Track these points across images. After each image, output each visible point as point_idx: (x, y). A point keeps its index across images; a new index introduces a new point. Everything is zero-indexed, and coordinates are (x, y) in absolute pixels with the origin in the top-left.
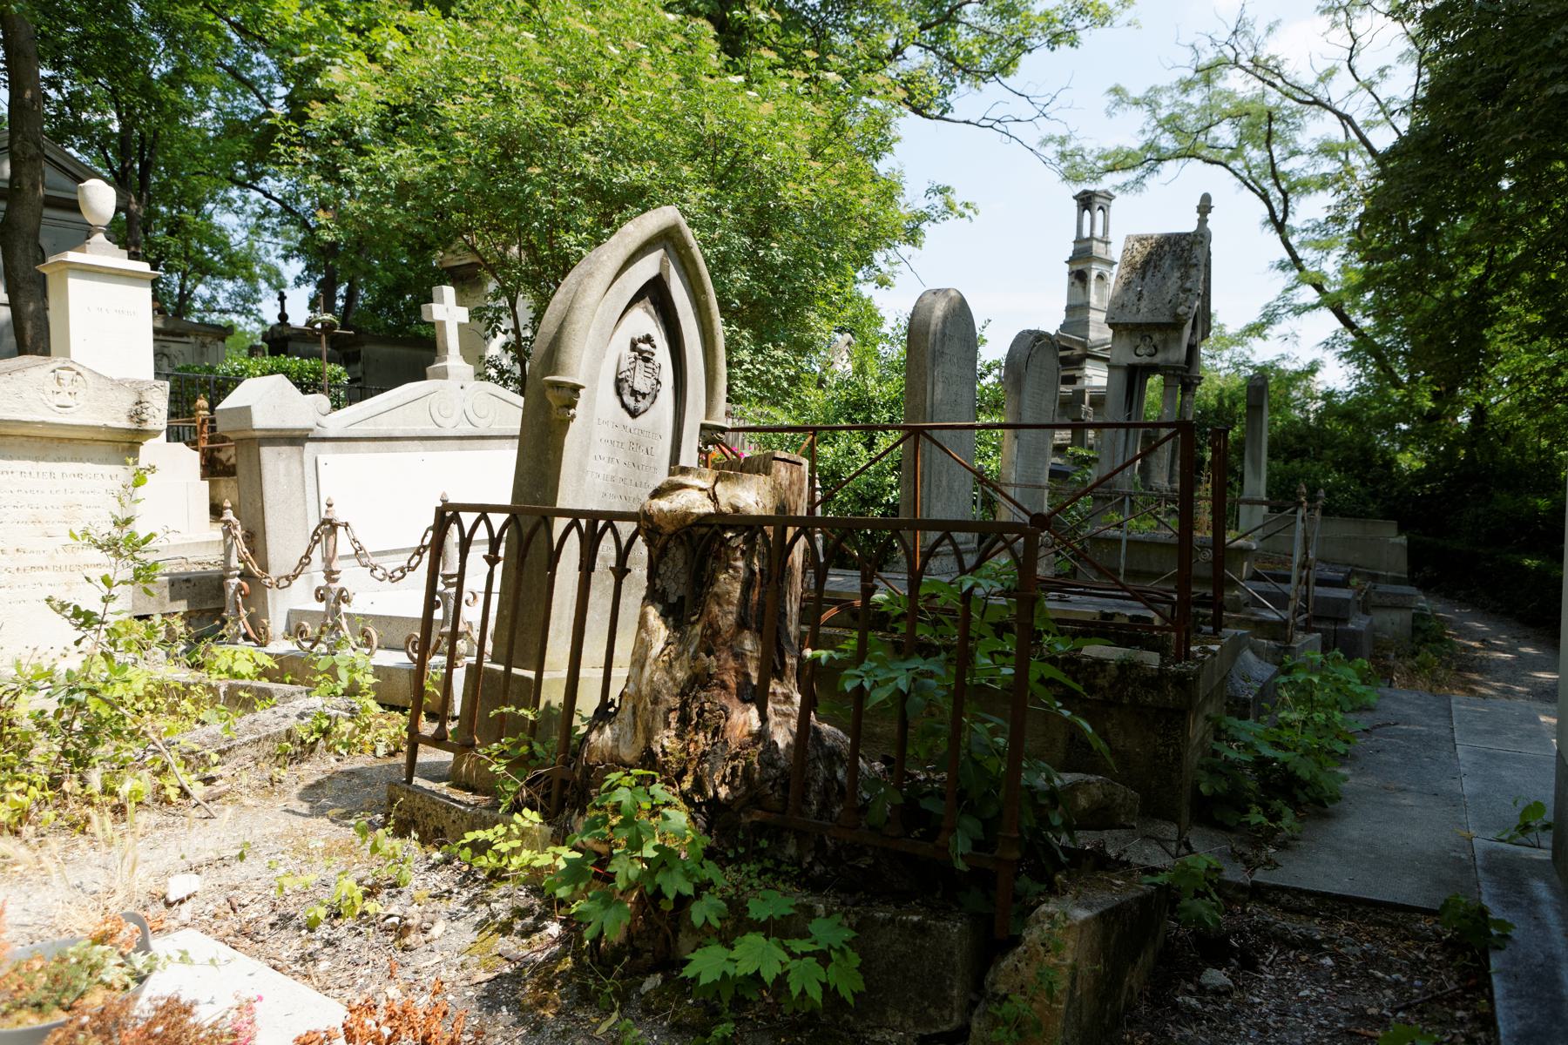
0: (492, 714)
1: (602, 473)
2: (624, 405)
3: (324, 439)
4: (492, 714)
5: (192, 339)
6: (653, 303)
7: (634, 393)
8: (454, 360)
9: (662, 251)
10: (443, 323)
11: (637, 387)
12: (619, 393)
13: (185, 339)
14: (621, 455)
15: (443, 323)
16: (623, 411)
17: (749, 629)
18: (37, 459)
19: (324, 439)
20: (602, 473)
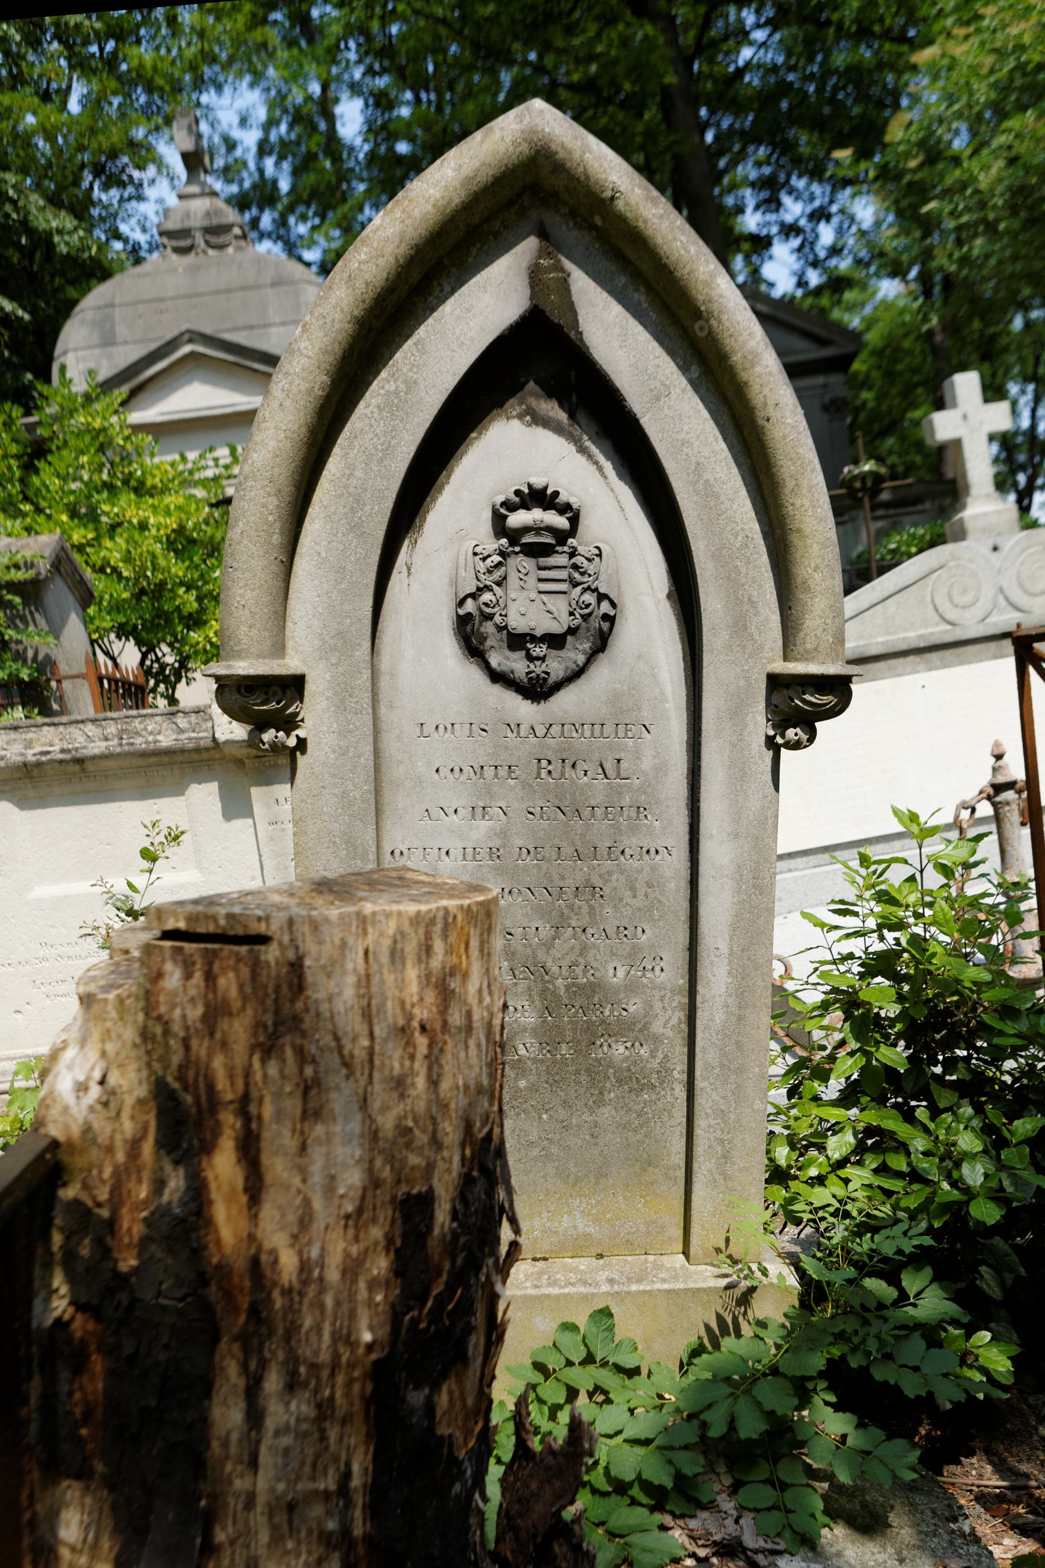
0: (1029, 1236)
1: (456, 846)
2: (497, 677)
3: (377, 752)
4: (1029, 1236)
5: (927, 505)
6: (551, 392)
7: (517, 641)
8: (984, 506)
9: (530, 245)
10: (957, 444)
11: (517, 623)
12: (473, 648)
13: (919, 507)
14: (511, 796)
15: (957, 444)
16: (497, 690)
17: (82, 1474)
18: (143, 797)
19: (377, 752)
20: (456, 846)
